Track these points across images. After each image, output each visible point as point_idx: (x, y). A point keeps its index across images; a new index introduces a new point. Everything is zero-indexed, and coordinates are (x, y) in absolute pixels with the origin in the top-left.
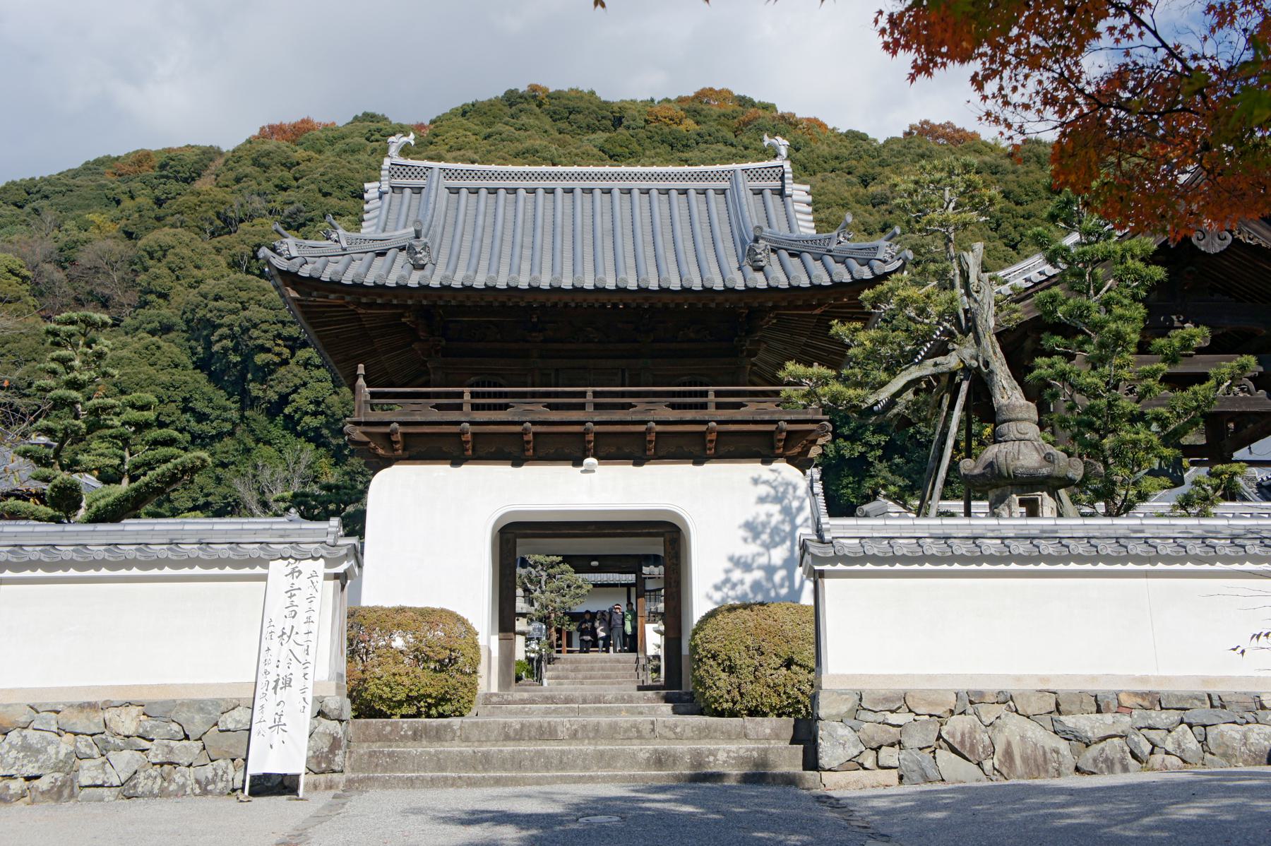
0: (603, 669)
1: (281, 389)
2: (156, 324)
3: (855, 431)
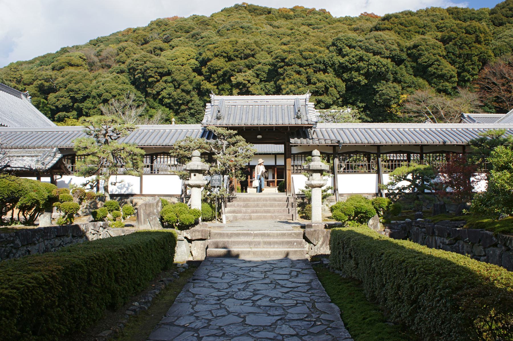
0: (265, 206)
1: (157, 90)
2: (119, 70)
3: (354, 101)
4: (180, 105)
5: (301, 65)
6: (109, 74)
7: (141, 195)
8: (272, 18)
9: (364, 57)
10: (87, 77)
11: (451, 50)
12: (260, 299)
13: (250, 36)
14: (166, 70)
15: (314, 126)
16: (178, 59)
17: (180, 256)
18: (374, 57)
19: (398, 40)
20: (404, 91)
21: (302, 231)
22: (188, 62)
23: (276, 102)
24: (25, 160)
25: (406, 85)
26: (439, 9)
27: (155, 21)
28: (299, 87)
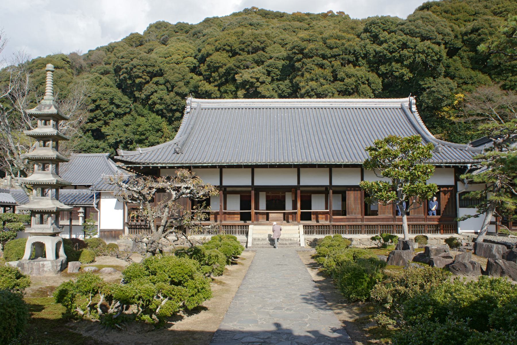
1: (146, 93)
2: (102, 71)
4: (173, 111)
5: (324, 57)
9: (409, 43)
10: (63, 79)
14: (156, 69)
16: (173, 57)
18: (422, 43)
22: (184, 60)
27: (154, 24)
28: (322, 85)
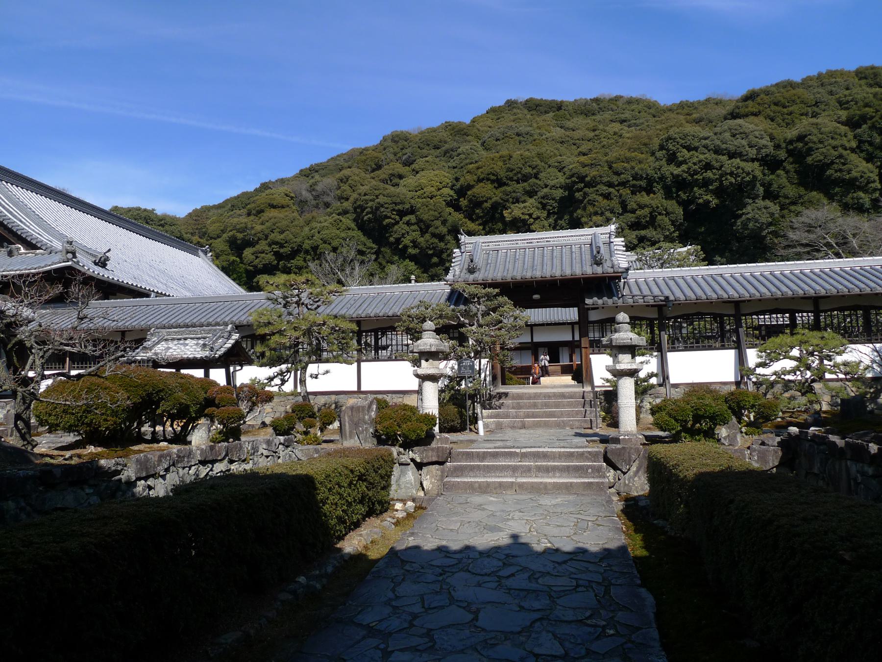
0: (547, 405)
5: (610, 185)
6: (327, 217)
7: (359, 392)
8: (564, 117)
9: (714, 163)
10: (296, 223)
11: (866, 137)
12: (513, 575)
13: (530, 147)
14: (407, 206)
15: (624, 275)
17: (403, 490)
19: (770, 131)
20: (786, 212)
21: (600, 448)
23: (562, 241)
24: (187, 345)
25: (787, 201)
26: (842, 73)
